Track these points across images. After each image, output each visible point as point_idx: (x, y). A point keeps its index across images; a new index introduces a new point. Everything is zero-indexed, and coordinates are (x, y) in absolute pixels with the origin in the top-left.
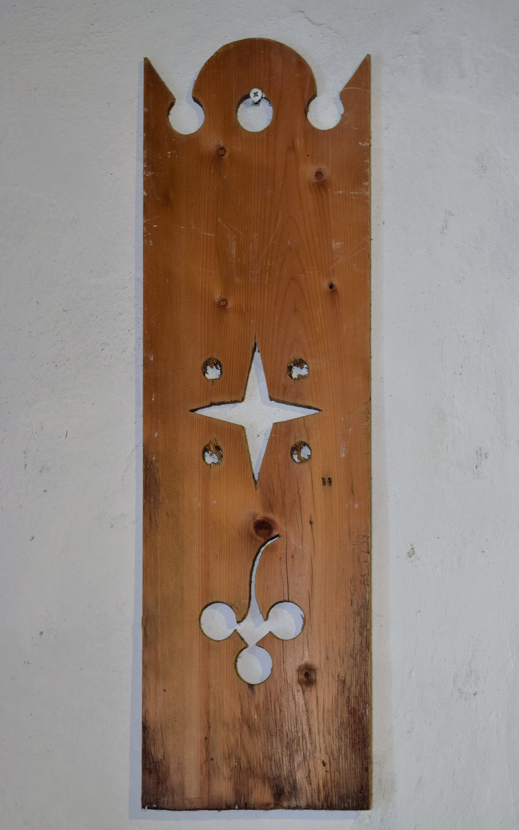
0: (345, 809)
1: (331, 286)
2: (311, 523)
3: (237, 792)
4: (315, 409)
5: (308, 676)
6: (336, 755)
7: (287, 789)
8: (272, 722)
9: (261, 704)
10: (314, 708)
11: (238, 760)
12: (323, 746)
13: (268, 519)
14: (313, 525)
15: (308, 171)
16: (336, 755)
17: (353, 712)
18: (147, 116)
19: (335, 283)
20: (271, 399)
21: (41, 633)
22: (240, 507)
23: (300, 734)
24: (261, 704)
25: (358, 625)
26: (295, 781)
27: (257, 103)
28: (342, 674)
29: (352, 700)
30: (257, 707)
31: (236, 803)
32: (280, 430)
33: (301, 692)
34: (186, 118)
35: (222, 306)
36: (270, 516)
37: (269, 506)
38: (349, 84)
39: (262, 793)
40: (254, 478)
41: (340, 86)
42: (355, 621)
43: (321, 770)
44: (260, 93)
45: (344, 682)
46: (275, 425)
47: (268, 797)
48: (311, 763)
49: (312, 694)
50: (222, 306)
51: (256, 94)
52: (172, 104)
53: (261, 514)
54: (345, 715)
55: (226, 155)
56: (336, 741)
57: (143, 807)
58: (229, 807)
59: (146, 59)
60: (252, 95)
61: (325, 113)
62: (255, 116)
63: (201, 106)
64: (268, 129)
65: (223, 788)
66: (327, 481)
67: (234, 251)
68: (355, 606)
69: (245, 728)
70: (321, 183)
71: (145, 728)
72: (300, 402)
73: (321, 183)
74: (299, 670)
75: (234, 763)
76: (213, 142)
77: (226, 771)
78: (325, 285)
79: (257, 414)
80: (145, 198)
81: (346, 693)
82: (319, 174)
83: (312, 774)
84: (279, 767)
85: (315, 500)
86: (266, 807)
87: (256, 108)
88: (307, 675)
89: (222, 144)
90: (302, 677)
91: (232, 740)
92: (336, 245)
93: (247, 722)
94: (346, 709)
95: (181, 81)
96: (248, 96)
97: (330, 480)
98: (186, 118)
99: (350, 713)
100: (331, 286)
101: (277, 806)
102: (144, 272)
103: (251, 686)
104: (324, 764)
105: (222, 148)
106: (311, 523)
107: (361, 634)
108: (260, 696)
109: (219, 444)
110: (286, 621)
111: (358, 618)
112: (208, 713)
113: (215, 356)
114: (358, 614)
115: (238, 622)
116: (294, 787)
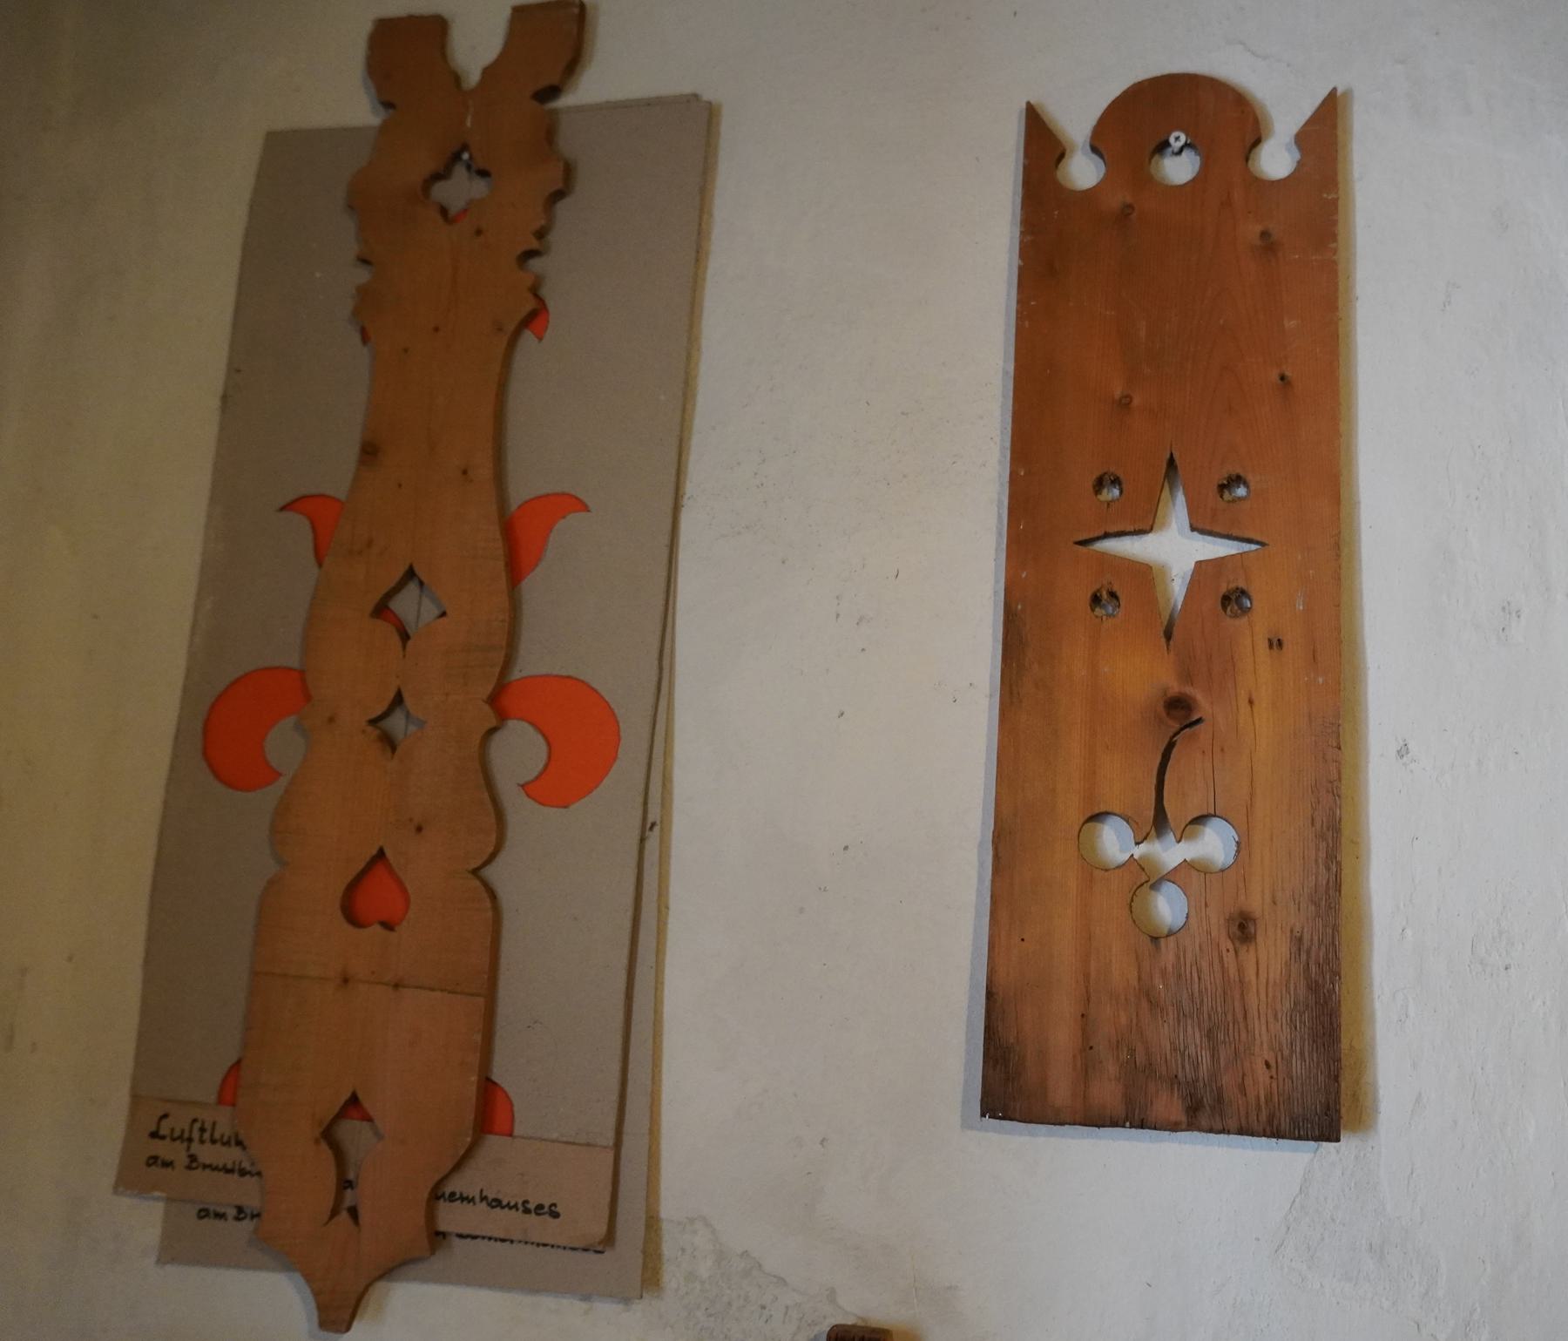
0: (1300, 1138)
1: (1283, 378)
2: (1251, 702)
3: (1158, 948)
4: (1257, 543)
5: (1243, 928)
6: (1286, 1052)
7: (1208, 1100)
8: (1185, 996)
9: (1170, 968)
10: (1253, 978)
11: (1132, 1051)
12: (1265, 1038)
13: (1195, 700)
14: (1256, 709)
15: (1250, 231)
16: (1286, 1052)
17: (1314, 987)
18: (1027, 171)
19: (1288, 373)
20: (1193, 529)
21: (846, 848)
22: (1140, 674)
23: (1230, 1018)
24: (1170, 968)
25: (1322, 855)
26: (1220, 1090)
27: (1180, 152)
28: (1297, 928)
29: (1313, 968)
30: (1164, 973)
31: (1126, 1119)
32: (1203, 570)
33: (1232, 952)
34: (1083, 171)
35: (1125, 404)
36: (1189, 690)
37: (1187, 676)
38: (1308, 123)
39: (1168, 1104)
40: (1107, 536)
41: (1295, 129)
42: (1318, 849)
43: (1262, 1075)
44: (1183, 138)
45: (1300, 939)
46: (1199, 564)
47: (1177, 1112)
48: (1247, 1064)
49: (1249, 957)
50: (1125, 404)
51: (1177, 139)
52: (1062, 156)
53: (1175, 688)
54: (1302, 992)
55: (1134, 215)
56: (1286, 1030)
57: (983, 1115)
58: (1115, 1124)
59: (1028, 104)
60: (1172, 140)
61: (1276, 160)
62: (1179, 168)
63: (1101, 156)
64: (1194, 180)
65: (1107, 1091)
66: (1276, 644)
67: (1143, 334)
68: (1318, 825)
69: (1145, 1004)
70: (1268, 245)
71: (990, 995)
72: (1235, 533)
73: (1268, 245)
74: (1230, 920)
75: (1124, 1056)
76: (1116, 200)
77: (1112, 1068)
78: (1274, 375)
79: (1175, 549)
80: (1020, 269)
81: (1304, 957)
82: (1265, 234)
83: (1249, 1082)
84: (1196, 1066)
85: (1259, 673)
86: (1174, 1127)
87: (1177, 159)
88: (1242, 927)
89: (1129, 199)
90: (1235, 929)
91: (1123, 1020)
92: (1290, 324)
93: (1147, 994)
94: (1302, 982)
95: (1076, 121)
96: (1166, 144)
97: (1280, 643)
98: (1083, 171)
99: (1309, 988)
100: (1283, 378)
101: (1192, 1126)
102: (1016, 360)
103: (1155, 939)
104: (1268, 1065)
105: (1130, 206)
106: (1251, 702)
107: (1328, 869)
108: (1168, 954)
109: (1116, 588)
110: (1215, 844)
111: (1323, 845)
112: (1087, 976)
113: (1112, 470)
114: (1322, 837)
115: (1137, 843)
116: (1220, 1099)
